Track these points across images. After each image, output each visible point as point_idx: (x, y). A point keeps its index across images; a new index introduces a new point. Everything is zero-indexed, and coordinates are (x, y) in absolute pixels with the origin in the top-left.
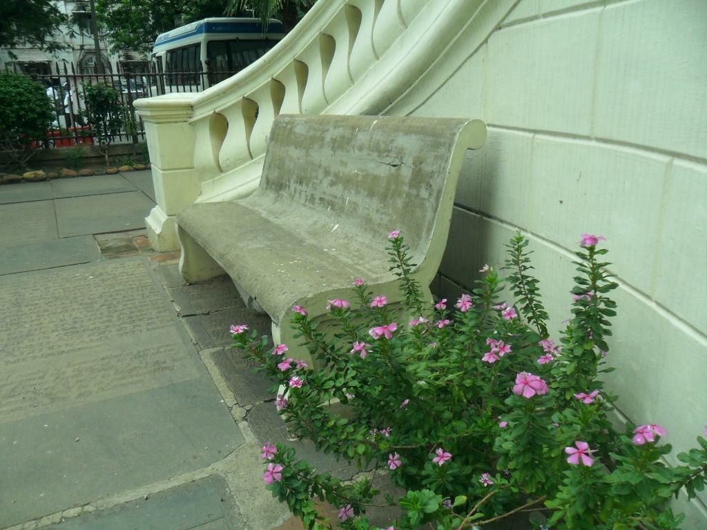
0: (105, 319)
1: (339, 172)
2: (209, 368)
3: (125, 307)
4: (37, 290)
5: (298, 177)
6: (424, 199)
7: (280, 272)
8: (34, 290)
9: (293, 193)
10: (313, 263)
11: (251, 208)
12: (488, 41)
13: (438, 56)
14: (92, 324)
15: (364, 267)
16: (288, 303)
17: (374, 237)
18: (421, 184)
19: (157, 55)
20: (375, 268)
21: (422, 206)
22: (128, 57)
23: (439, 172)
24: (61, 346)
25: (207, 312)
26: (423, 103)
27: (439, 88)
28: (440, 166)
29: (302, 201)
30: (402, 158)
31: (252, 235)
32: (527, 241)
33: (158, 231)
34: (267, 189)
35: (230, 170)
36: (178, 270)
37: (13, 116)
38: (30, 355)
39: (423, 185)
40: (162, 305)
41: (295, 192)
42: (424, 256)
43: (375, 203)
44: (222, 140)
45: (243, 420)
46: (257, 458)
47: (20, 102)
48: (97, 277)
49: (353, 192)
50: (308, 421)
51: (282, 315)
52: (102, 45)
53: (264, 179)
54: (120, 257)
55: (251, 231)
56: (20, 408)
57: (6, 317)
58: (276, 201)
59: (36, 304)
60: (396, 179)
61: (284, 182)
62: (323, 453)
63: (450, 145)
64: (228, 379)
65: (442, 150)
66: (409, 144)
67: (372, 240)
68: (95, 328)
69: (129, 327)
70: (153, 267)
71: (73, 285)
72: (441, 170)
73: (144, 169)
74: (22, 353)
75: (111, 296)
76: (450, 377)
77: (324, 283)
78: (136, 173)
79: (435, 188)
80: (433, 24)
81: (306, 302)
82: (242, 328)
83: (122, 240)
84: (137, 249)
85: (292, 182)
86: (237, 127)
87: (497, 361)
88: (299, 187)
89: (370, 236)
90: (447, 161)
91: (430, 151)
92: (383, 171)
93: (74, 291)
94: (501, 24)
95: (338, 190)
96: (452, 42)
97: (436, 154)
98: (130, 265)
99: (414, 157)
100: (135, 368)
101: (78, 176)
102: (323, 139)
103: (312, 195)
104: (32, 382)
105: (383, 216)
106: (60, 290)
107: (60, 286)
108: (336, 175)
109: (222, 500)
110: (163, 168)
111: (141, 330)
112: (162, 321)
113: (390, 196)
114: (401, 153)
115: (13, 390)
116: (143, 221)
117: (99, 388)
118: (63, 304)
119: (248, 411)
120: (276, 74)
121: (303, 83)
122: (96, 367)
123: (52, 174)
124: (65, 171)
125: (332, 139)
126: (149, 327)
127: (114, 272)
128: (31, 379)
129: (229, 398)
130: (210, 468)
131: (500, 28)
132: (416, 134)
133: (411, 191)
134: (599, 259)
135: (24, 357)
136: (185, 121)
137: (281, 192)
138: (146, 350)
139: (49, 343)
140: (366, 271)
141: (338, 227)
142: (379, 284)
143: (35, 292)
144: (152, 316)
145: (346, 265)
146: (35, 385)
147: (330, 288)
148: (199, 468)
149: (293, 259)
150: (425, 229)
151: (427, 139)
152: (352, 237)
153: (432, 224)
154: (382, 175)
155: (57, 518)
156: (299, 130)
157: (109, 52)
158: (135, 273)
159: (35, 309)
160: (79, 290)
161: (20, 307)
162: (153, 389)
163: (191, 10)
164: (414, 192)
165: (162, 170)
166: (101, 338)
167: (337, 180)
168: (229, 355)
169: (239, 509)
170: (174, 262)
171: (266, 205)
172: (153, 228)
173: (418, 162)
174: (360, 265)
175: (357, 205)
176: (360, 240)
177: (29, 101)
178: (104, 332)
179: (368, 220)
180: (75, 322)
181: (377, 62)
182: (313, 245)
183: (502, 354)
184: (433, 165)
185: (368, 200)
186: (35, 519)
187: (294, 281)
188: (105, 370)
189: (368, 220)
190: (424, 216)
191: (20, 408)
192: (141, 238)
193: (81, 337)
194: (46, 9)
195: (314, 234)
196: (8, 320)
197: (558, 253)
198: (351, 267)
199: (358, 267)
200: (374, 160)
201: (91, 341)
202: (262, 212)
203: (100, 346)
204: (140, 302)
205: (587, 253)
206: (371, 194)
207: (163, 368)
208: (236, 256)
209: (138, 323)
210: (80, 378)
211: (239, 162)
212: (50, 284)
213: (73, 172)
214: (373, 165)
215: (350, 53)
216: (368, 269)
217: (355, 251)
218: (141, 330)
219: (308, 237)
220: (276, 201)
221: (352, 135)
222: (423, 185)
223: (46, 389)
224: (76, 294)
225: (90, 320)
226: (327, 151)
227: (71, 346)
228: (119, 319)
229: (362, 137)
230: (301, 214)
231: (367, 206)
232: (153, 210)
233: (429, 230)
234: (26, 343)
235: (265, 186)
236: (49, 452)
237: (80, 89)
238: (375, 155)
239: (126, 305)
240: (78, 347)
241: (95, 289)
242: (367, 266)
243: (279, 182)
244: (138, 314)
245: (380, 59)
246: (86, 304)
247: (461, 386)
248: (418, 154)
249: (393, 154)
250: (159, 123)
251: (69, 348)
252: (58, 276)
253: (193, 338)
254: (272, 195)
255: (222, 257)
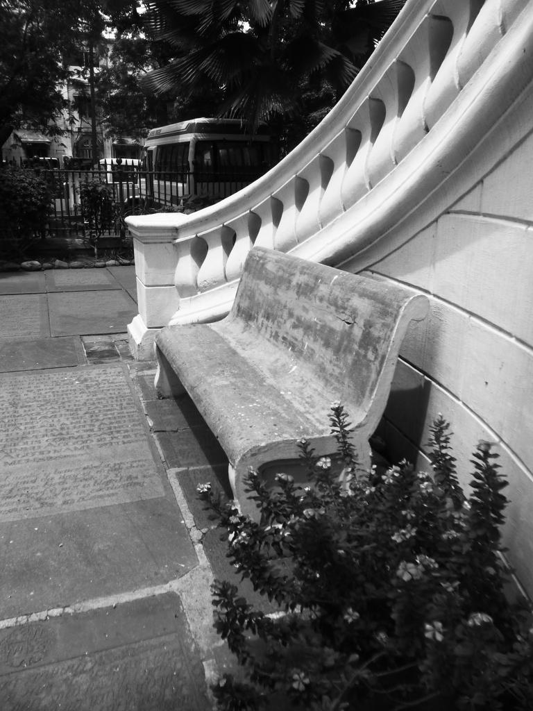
0: (88, 428)
1: (302, 316)
2: (174, 488)
3: (105, 417)
4: (31, 391)
5: (265, 312)
6: (370, 361)
7: (240, 415)
8: (28, 391)
9: (260, 326)
10: (269, 408)
11: (222, 334)
12: (439, 220)
13: (396, 223)
14: (77, 432)
15: (314, 416)
16: (243, 449)
17: (326, 386)
18: (369, 347)
19: (149, 149)
20: (323, 418)
21: (368, 367)
22: (121, 141)
23: (385, 340)
24: (49, 452)
25: (176, 430)
26: (381, 260)
27: (396, 250)
28: (386, 334)
29: (268, 336)
30: (355, 318)
31: (220, 369)
32: (448, 424)
33: (138, 342)
34: (237, 316)
35: (206, 290)
36: (153, 382)
37: (17, 208)
38: (25, 458)
39: (371, 348)
40: (137, 418)
41: (262, 326)
42: (366, 414)
43: (329, 354)
44: (200, 267)
45: (199, 543)
46: (208, 580)
47: (24, 196)
48: (82, 382)
49: (312, 339)
50: (248, 558)
51: (238, 460)
52: (98, 129)
53: (236, 306)
54: (102, 363)
55: (220, 364)
56: (15, 510)
57: (5, 417)
58: (245, 330)
59: (30, 406)
60: (348, 335)
61: (253, 313)
62: (259, 594)
63: (396, 316)
64: (189, 501)
65: (389, 320)
66: (363, 306)
67: (324, 389)
68: (79, 436)
69: (108, 438)
70: (132, 376)
71: (62, 389)
72: (387, 337)
73: (129, 264)
74: (18, 456)
75: (94, 404)
76: (366, 547)
77: (276, 432)
78: (121, 268)
79: (380, 353)
80: (392, 195)
81: (259, 450)
82: (206, 486)
83: (106, 344)
84: (118, 355)
85: (260, 315)
86: (215, 253)
87: (403, 541)
88: (266, 322)
89: (322, 384)
90: (392, 330)
91: (379, 317)
92: (338, 326)
93: (62, 395)
94: (450, 210)
95: (298, 333)
96: (408, 215)
97: (383, 321)
98: (111, 376)
99: (365, 320)
100: (110, 481)
101: (69, 268)
102: (290, 282)
103: (277, 333)
104: (26, 485)
105: (335, 368)
106: (51, 394)
107: (50, 389)
108: (298, 319)
109: (176, 616)
110: (148, 284)
111: (118, 443)
112: (136, 435)
113: (342, 350)
114: (354, 313)
115: (11, 491)
116: (126, 325)
117: (80, 498)
118: (52, 408)
119: (204, 534)
120: (255, 208)
121: (277, 220)
122: (79, 477)
123: (46, 265)
124: (58, 262)
125: (297, 284)
126: (126, 440)
127: (97, 379)
128: (24, 483)
129: (188, 520)
130: (168, 585)
131: (449, 213)
132: (368, 298)
133: (360, 351)
134: (491, 461)
135: (19, 459)
136: (170, 242)
137: (249, 323)
138: (121, 463)
139: (39, 447)
140: (314, 422)
141: (296, 369)
142: (323, 437)
143: (29, 393)
144: (128, 429)
145: (298, 412)
146: (28, 488)
147: (280, 439)
148: (159, 584)
149: (253, 401)
150: (369, 388)
151: (377, 305)
152: (307, 382)
153: (375, 386)
154: (338, 329)
155: (43, 615)
156: (270, 267)
157: (104, 136)
158: (115, 381)
159: (29, 410)
160: (67, 395)
161: (16, 408)
162: (125, 503)
163: (184, 100)
164: (362, 352)
165: (146, 286)
166: (83, 447)
167: (298, 324)
168: (192, 476)
169: (189, 627)
170: (150, 372)
171: (232, 331)
172: (134, 337)
173: (369, 325)
174: (310, 413)
175: (314, 352)
176: (314, 386)
177: (31, 195)
178: (87, 441)
179: (322, 369)
180: (62, 429)
181: (344, 213)
182: (272, 386)
183: (408, 536)
184: (380, 331)
185: (324, 350)
186: (26, 615)
187: (251, 427)
188: (86, 480)
189: (322, 369)
190: (369, 377)
191: (15, 510)
192: (122, 343)
193: (67, 444)
194: (51, 94)
195: (275, 373)
196: (6, 420)
197: (482, 427)
198: (302, 414)
199: (309, 416)
200: (331, 313)
201: (76, 449)
202: (232, 340)
203: (82, 455)
204: (119, 413)
205: (482, 454)
206: (327, 344)
207: (135, 483)
208: (204, 391)
209: (116, 435)
210: (66, 486)
211: (214, 284)
212: (42, 386)
213: (65, 264)
214: (330, 318)
215: (321, 199)
216: (317, 419)
217: (308, 397)
218: (118, 443)
219: (268, 376)
220: (245, 330)
221: (315, 284)
222: (371, 348)
223: (37, 494)
224: (63, 398)
225: (75, 427)
226: (292, 294)
227: (58, 452)
228: (100, 429)
229: (323, 290)
230: (265, 349)
231: (322, 355)
232: (135, 318)
233: (372, 390)
234: (21, 445)
235: (236, 313)
236: (39, 554)
237: (77, 185)
238: (333, 308)
239: (106, 415)
240: (63, 454)
241: (80, 395)
242: (317, 416)
243: (248, 312)
244: (116, 425)
245: (347, 211)
246: (72, 410)
247: (374, 555)
248: (368, 318)
249: (347, 312)
250: (146, 243)
251: (56, 454)
252: (49, 379)
253: (162, 456)
254: (241, 324)
255: (192, 388)
